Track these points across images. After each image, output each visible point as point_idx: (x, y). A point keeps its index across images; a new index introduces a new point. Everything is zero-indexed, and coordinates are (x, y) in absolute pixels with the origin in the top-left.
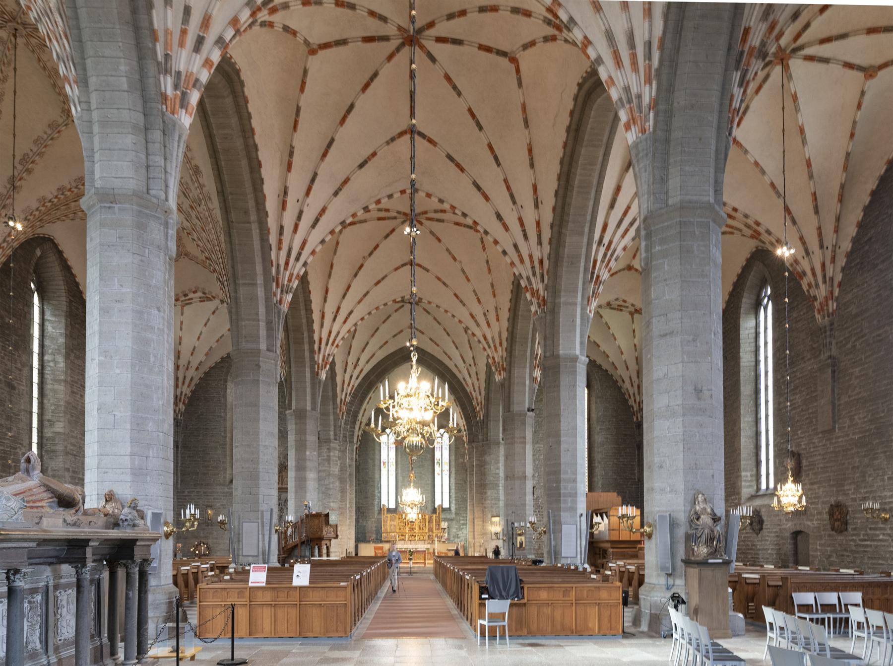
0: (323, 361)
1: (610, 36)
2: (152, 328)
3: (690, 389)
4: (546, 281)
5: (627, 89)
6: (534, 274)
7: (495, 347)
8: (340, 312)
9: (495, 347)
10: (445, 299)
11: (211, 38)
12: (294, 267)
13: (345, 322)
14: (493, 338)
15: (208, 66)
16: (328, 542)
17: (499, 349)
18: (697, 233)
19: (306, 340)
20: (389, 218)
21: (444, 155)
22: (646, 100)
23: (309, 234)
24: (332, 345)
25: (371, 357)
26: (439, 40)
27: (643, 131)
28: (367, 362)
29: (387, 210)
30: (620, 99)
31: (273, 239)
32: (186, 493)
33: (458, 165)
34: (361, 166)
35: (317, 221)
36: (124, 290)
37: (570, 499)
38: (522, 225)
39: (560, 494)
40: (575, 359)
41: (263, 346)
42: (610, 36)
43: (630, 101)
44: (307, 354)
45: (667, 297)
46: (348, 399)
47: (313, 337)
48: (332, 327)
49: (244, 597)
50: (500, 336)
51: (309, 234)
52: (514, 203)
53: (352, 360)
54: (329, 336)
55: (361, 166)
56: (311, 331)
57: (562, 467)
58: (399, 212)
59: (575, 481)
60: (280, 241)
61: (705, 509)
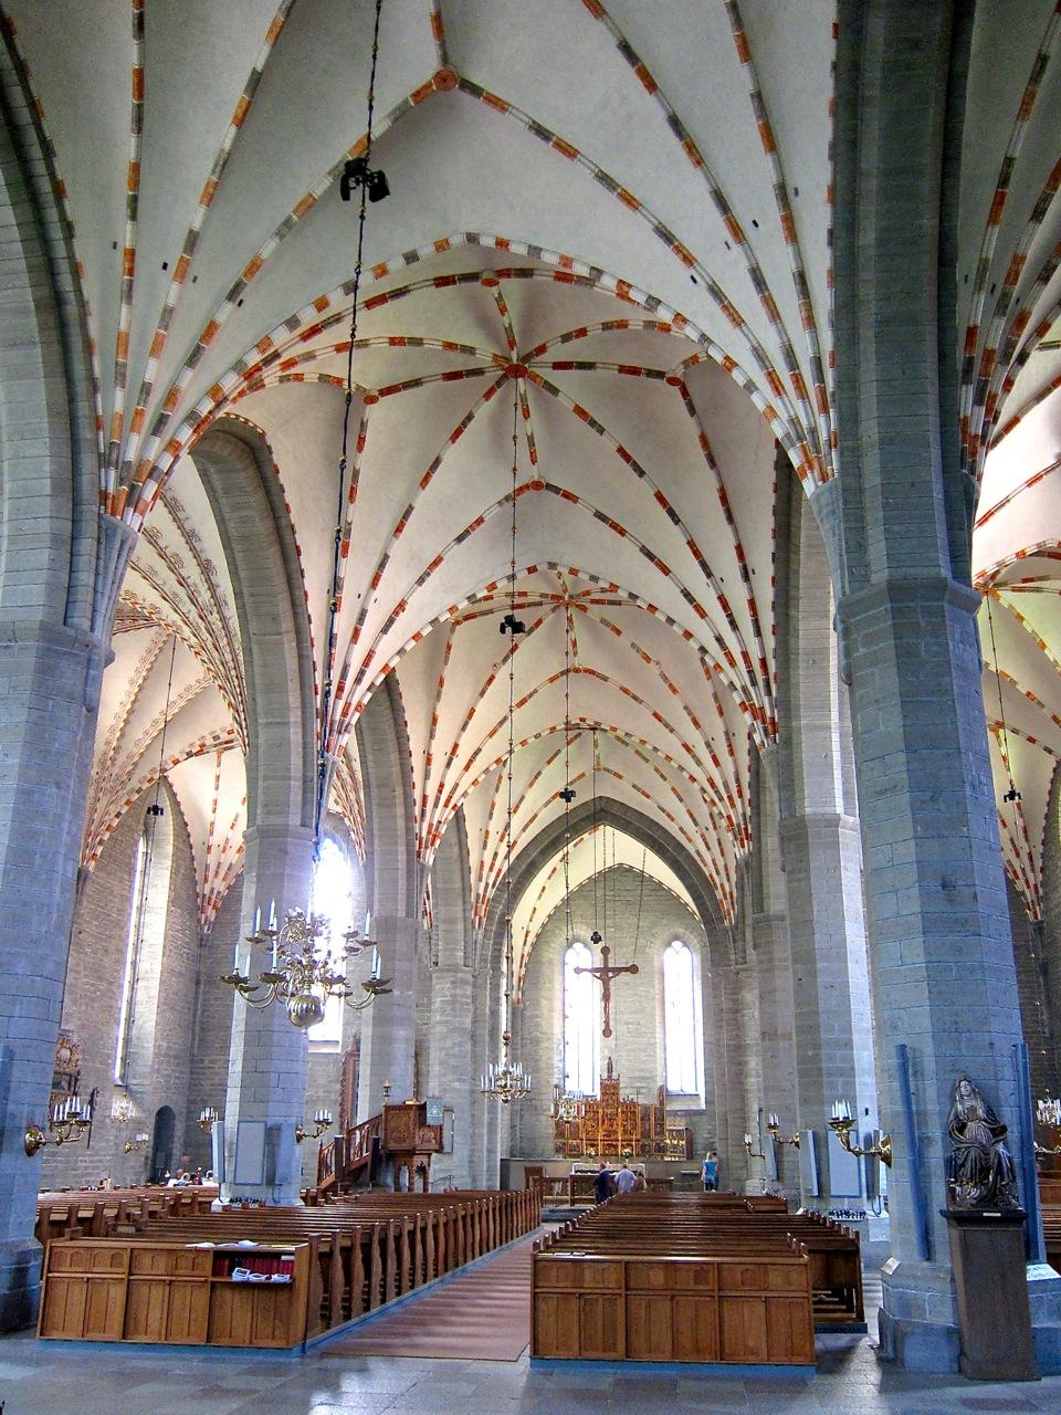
0: (429, 832)
1: (759, 354)
2: (44, 814)
3: (935, 885)
4: (774, 694)
5: (794, 421)
6: (754, 683)
7: (730, 798)
8: (459, 751)
9: (730, 798)
10: (641, 725)
11: (178, 414)
12: (352, 693)
13: (467, 768)
14: (726, 785)
15: (172, 449)
16: (425, 1159)
17: (738, 801)
18: (923, 624)
19: (399, 800)
20: (529, 605)
21: (653, 493)
22: (823, 436)
23: (377, 641)
24: (446, 805)
25: (531, 821)
26: (558, 366)
27: (824, 478)
28: (524, 830)
29: (524, 594)
30: (787, 435)
31: (318, 654)
32: (206, 1064)
33: (614, 526)
34: (460, 539)
35: (391, 622)
36: (9, 761)
37: (841, 1079)
38: (725, 606)
39: (820, 1069)
40: (834, 822)
41: (294, 820)
42: (759, 354)
43: (800, 438)
44: (401, 823)
45: (882, 728)
46: (491, 893)
47: (412, 795)
48: (444, 776)
49: (121, 1265)
50: (738, 780)
51: (377, 641)
52: (709, 575)
53: (496, 826)
54: (440, 791)
55: (460, 539)
56: (408, 785)
57: (823, 1018)
58: (542, 595)
59: (848, 1044)
60: (329, 657)
61: (973, 1109)
